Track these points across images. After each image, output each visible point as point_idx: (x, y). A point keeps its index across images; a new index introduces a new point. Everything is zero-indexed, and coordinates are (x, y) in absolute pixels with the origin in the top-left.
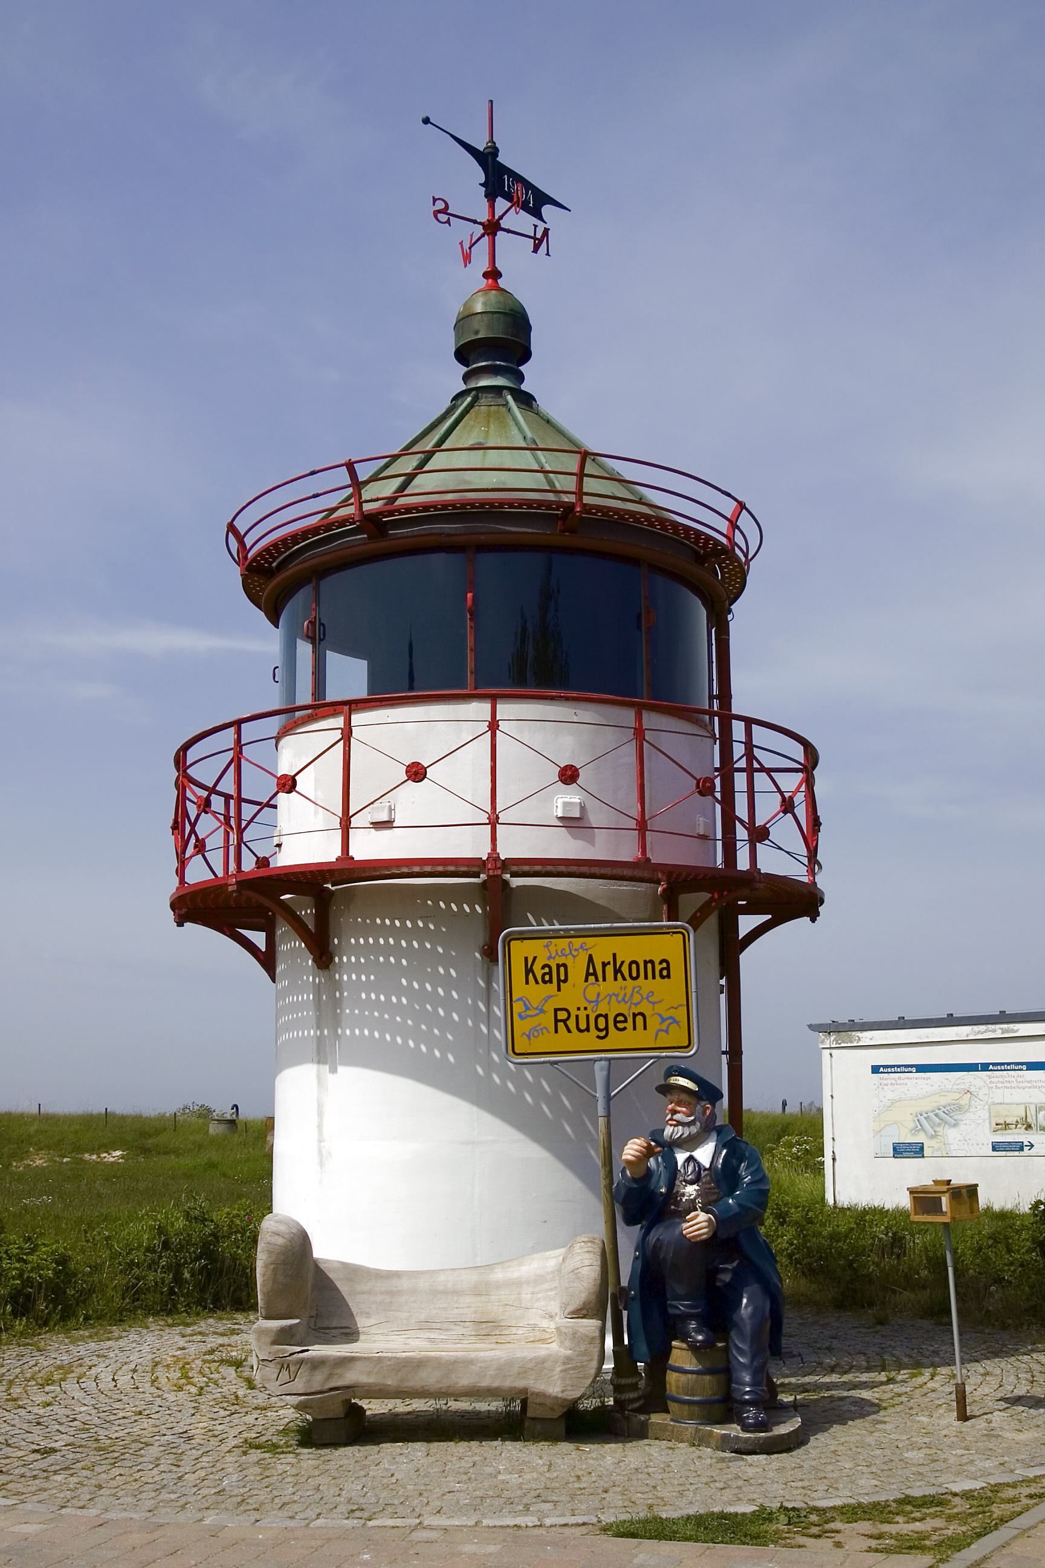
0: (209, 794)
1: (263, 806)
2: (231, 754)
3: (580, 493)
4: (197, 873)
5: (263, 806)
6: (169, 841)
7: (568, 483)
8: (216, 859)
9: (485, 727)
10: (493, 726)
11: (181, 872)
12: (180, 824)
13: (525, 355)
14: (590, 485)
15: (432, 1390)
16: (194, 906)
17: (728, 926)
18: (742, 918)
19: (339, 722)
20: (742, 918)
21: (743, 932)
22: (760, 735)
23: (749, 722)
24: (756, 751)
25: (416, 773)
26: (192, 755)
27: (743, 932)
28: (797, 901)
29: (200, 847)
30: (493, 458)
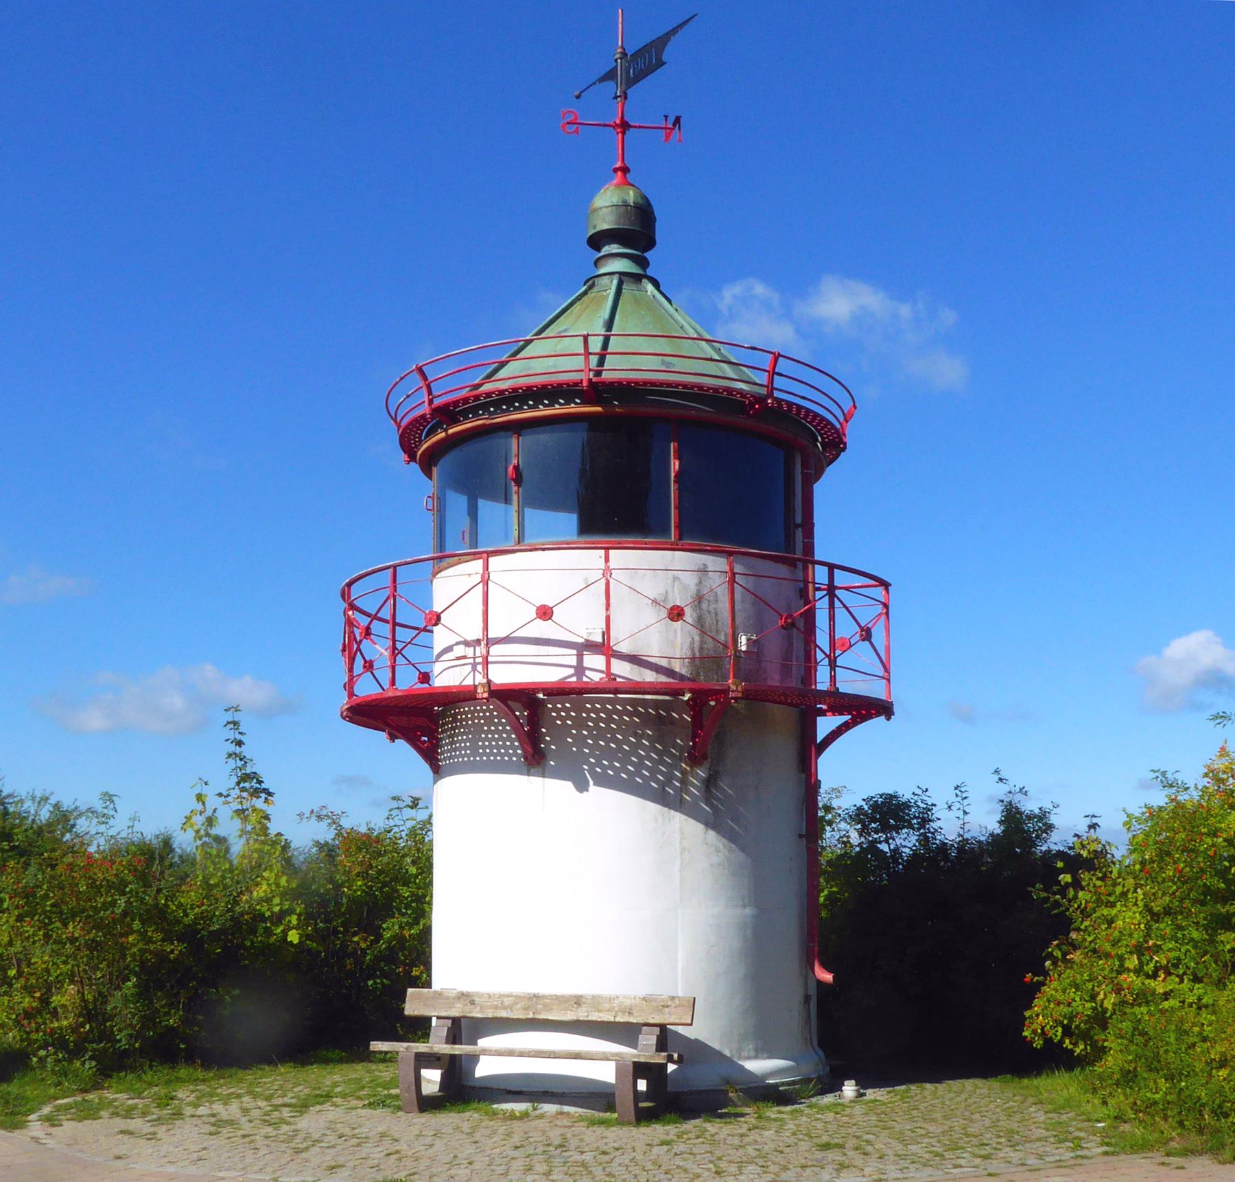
0: (376, 615)
1: (420, 630)
2: (387, 592)
3: (771, 388)
4: (367, 688)
5: (420, 630)
6: (342, 662)
7: (762, 378)
8: (384, 676)
9: (599, 574)
10: (607, 572)
11: (350, 687)
12: (350, 650)
13: (650, 243)
14: (779, 382)
15: (502, 433)
16: (365, 713)
17: (809, 728)
18: (820, 720)
19: (478, 565)
20: (820, 720)
21: (821, 735)
22: (841, 578)
23: (832, 567)
24: (837, 592)
25: (545, 614)
26: (356, 591)
27: (821, 735)
28: (864, 709)
29: (369, 666)
30: (687, 348)
